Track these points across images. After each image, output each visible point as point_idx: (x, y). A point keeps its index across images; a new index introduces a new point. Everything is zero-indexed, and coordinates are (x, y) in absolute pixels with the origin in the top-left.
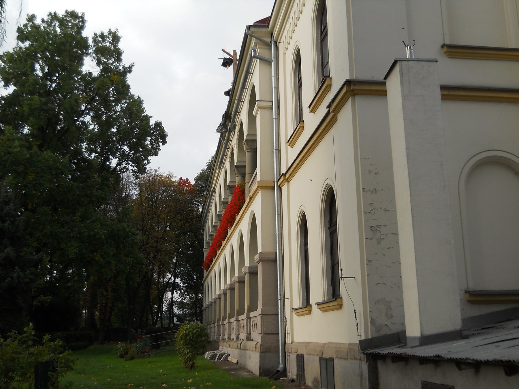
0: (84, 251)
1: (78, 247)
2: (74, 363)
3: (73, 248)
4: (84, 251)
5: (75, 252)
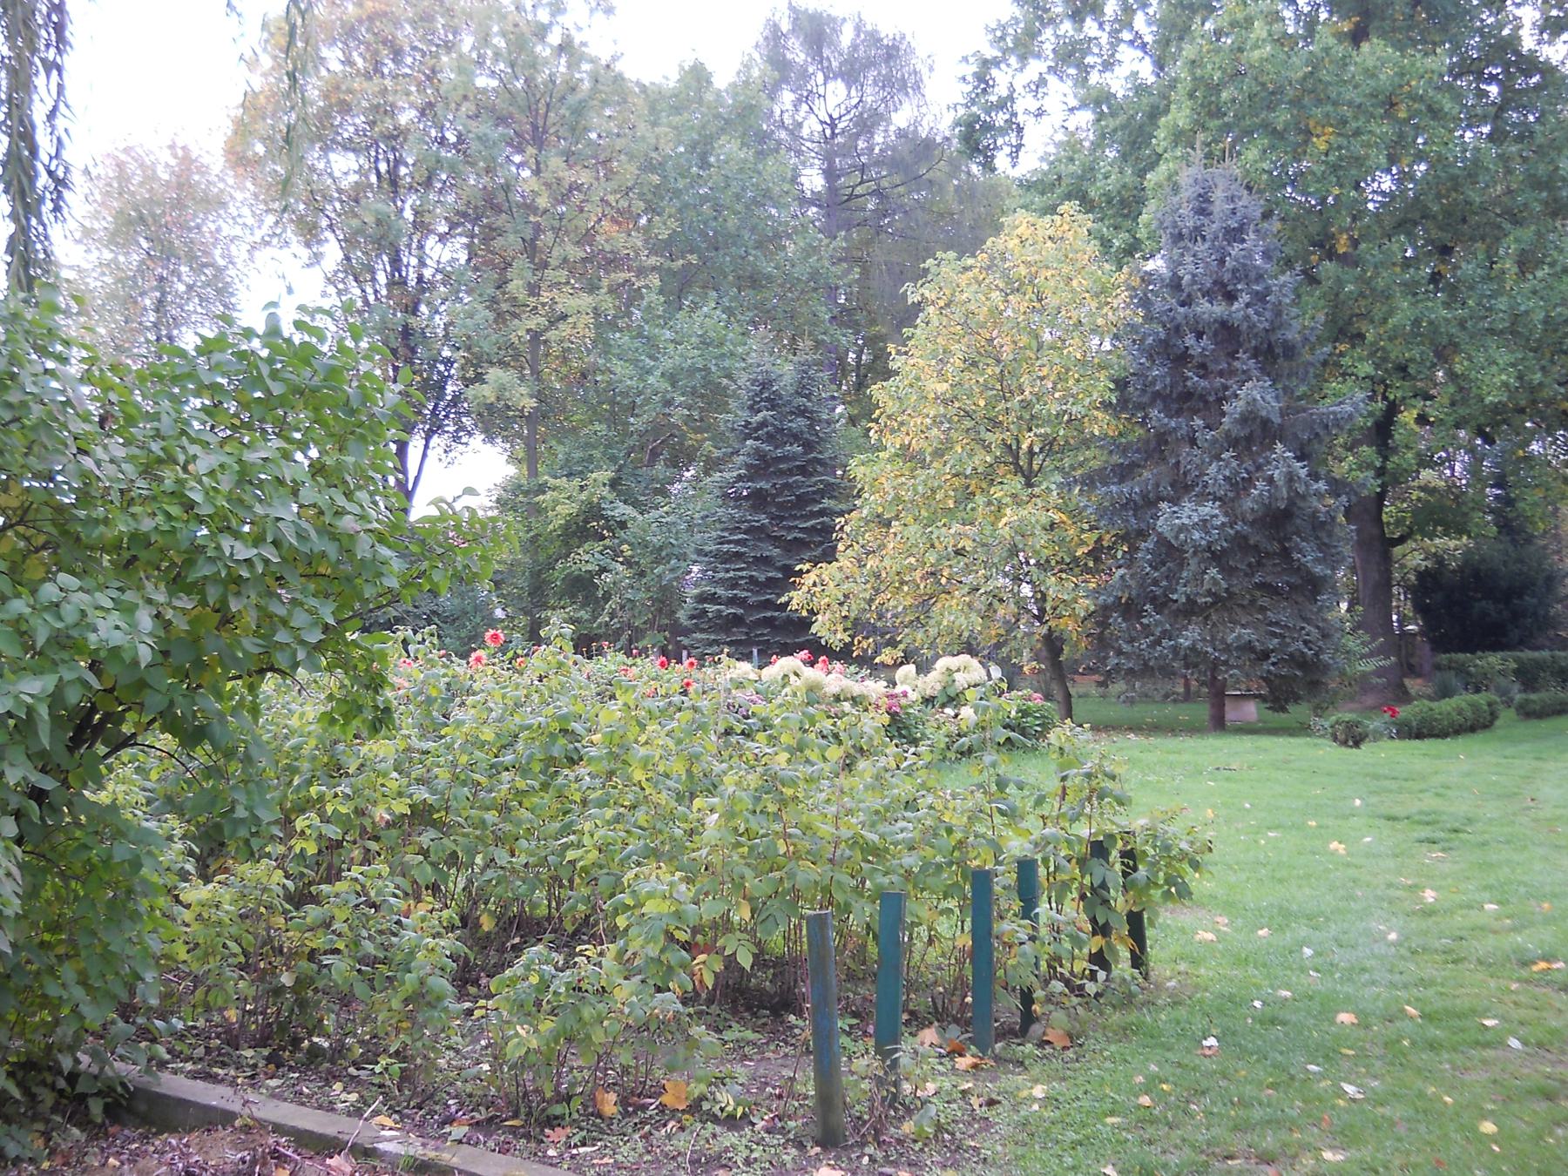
0: (1538, 377)
1: (1513, 365)
2: (1196, 865)
3: (1494, 369)
4: (1538, 377)
5: (1505, 384)
